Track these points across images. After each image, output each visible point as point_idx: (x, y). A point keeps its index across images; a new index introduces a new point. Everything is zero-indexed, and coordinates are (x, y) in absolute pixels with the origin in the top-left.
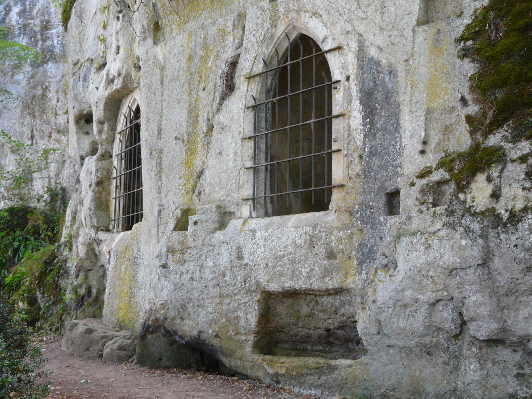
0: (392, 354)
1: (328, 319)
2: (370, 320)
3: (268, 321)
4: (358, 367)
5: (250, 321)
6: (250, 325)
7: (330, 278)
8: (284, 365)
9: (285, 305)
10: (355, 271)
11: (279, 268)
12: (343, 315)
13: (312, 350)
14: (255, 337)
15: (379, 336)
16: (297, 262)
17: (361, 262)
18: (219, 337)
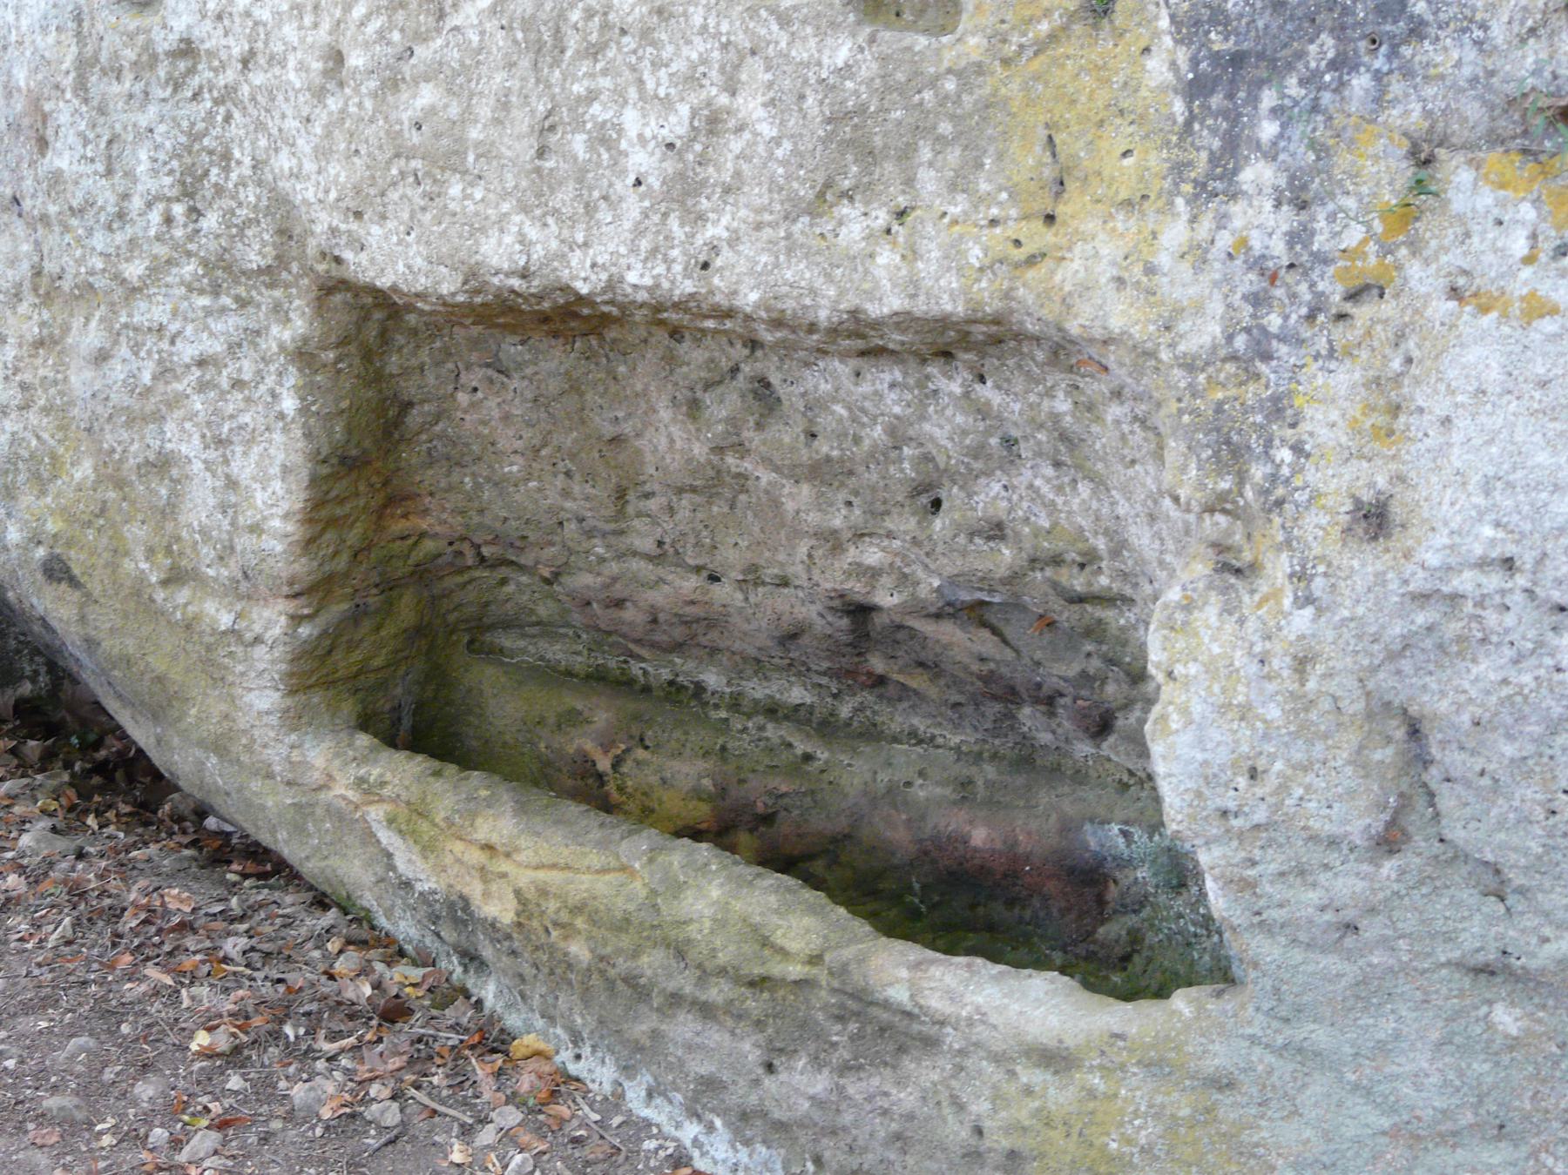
0: (1513, 1044)
1: (859, 536)
2: (1301, 704)
3: (395, 498)
4: (1136, 1090)
5: (249, 498)
6: (256, 529)
7: (882, 217)
8: (504, 866)
9: (515, 383)
10: (1157, 161)
11: (427, 95)
12: (996, 531)
13: (735, 704)
14: (296, 619)
15: (1389, 867)
16: (573, 43)
17: (1237, 60)
18: (74, 582)
